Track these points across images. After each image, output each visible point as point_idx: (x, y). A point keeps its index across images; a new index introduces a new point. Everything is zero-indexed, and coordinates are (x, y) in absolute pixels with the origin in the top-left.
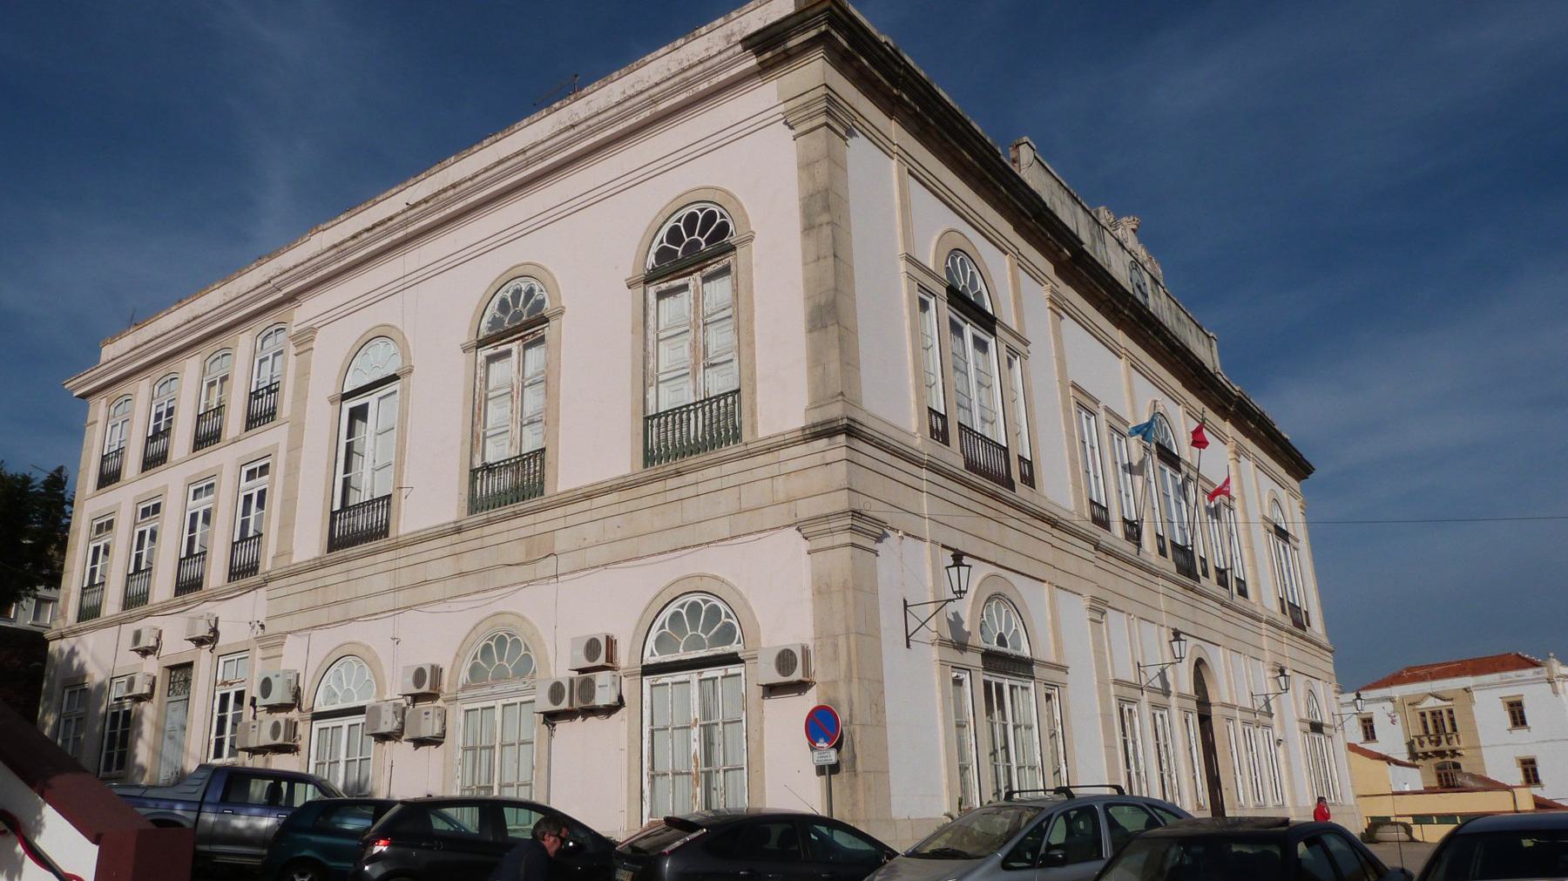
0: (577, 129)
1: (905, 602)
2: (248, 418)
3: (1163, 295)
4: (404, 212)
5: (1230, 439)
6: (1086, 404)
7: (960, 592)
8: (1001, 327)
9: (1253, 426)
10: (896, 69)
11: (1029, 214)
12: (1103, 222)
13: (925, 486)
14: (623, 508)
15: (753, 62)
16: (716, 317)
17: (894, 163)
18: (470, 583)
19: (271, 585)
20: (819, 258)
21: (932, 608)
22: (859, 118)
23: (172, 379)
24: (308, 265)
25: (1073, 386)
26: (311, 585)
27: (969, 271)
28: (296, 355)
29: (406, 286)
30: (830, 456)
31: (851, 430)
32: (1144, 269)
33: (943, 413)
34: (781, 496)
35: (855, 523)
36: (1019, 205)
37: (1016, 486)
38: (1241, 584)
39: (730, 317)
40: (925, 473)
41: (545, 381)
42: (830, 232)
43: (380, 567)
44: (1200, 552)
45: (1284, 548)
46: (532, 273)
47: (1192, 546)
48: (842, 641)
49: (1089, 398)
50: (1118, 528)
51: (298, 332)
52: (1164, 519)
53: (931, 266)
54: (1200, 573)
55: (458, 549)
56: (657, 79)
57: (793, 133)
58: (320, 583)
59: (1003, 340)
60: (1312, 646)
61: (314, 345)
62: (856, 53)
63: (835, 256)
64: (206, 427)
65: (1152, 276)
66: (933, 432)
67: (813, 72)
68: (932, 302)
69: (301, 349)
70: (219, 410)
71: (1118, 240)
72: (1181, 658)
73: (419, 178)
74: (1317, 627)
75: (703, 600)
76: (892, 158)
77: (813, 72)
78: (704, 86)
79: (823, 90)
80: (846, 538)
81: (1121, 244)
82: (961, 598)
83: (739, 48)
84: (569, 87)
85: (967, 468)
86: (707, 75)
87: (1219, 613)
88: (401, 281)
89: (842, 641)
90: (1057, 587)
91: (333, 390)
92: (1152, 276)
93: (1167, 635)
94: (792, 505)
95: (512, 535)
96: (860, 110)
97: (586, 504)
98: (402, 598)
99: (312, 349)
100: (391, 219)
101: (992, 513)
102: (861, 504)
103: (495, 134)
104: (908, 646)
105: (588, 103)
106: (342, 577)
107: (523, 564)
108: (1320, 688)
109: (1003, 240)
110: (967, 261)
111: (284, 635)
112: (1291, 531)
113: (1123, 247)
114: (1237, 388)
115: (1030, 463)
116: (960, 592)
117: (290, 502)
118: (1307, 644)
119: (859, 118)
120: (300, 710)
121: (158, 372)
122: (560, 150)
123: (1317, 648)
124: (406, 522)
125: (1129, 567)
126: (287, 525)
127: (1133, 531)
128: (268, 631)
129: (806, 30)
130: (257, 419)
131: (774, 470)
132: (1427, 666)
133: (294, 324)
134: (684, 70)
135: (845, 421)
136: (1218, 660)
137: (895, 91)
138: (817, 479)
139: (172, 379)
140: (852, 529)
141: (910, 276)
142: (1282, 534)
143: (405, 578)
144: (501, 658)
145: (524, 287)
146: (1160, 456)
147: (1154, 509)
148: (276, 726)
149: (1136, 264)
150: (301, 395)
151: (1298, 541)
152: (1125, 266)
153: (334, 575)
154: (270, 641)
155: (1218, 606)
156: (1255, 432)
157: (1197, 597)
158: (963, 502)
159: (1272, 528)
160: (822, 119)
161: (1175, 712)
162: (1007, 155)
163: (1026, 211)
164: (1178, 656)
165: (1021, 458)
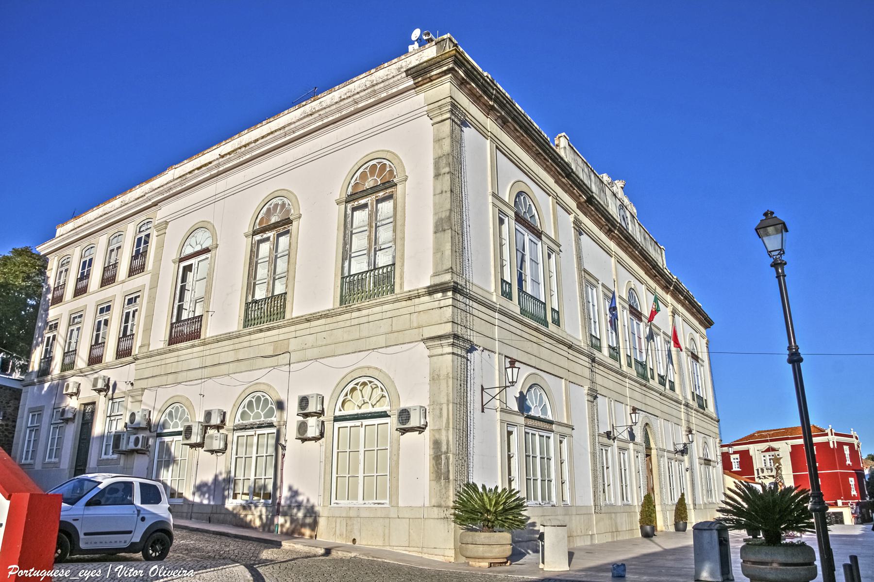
0: (313, 116)
1: (482, 386)
2: (130, 268)
3: (637, 225)
4: (217, 159)
5: (670, 305)
6: (587, 279)
7: (636, 423)
8: (545, 236)
9: (682, 298)
10: (491, 91)
11: (563, 174)
12: (605, 183)
13: (497, 322)
14: (327, 328)
15: (411, 82)
16: (384, 222)
17: (488, 142)
18: (242, 366)
19: (138, 362)
20: (442, 192)
21: (497, 390)
22: (469, 116)
23: (92, 248)
24: (165, 187)
25: (584, 271)
26: (159, 363)
27: (528, 204)
28: (157, 236)
29: (216, 200)
30: (443, 303)
31: (456, 289)
32: (627, 209)
33: (544, 302)
34: (415, 325)
35: (455, 341)
36: (558, 169)
37: (549, 325)
38: (672, 384)
39: (392, 222)
40: (497, 315)
41: (289, 255)
42: (449, 178)
43: (195, 355)
44: (650, 365)
45: (696, 365)
46: (284, 195)
47: (646, 362)
48: (445, 407)
49: (593, 278)
50: (606, 351)
51: (158, 224)
52: (632, 348)
53: (507, 200)
54: (649, 377)
55: (237, 346)
56: (358, 90)
57: (432, 122)
58: (163, 362)
59: (546, 243)
60: (708, 418)
61: (167, 231)
62: (468, 80)
63: (451, 191)
64: (108, 274)
65: (631, 214)
66: (503, 293)
67: (444, 88)
68: (506, 220)
69: (160, 233)
70: (115, 265)
71: (613, 193)
72: (636, 423)
73: (228, 141)
74: (711, 409)
75: (369, 381)
76: (488, 139)
77: (444, 88)
78: (384, 95)
79: (449, 100)
80: (449, 349)
81: (615, 195)
82: (513, 386)
83: (404, 75)
84: (313, 93)
85: (521, 313)
86: (385, 88)
87: (659, 399)
88: (214, 198)
89: (445, 407)
90: (569, 381)
91: (175, 256)
92: (631, 214)
93: (629, 410)
94: (421, 329)
95: (267, 340)
96: (470, 112)
97: (307, 325)
98: (206, 372)
99: (165, 233)
100: (210, 163)
101: (534, 339)
102: (460, 331)
103: (269, 118)
104: (483, 411)
105: (321, 103)
106: (175, 359)
107: (272, 356)
108: (711, 441)
109: (538, 178)
110: (527, 199)
111: (143, 390)
112: (700, 356)
113: (616, 197)
114: (675, 277)
115: (558, 312)
116: (513, 382)
117: (150, 317)
118: (706, 417)
119: (469, 116)
120: (150, 431)
121: (85, 243)
122: (303, 127)
123: (710, 419)
124: (209, 331)
125: (610, 372)
126: (148, 329)
127: (615, 352)
128: (135, 387)
129: (441, 67)
130: (135, 271)
131: (412, 309)
132: (768, 431)
133: (157, 219)
134: (373, 86)
135: (452, 284)
136: (658, 425)
137: (490, 103)
138: (436, 315)
139: (92, 248)
140: (453, 345)
141: (494, 205)
142: (695, 357)
143: (209, 361)
144: (258, 409)
145: (280, 202)
146: (631, 312)
147: (626, 341)
148: (137, 439)
149: (622, 206)
150: (158, 260)
151: (703, 361)
152: (616, 207)
153: (171, 358)
154: (136, 394)
155: (658, 395)
156: (683, 301)
157: (647, 390)
158: (518, 332)
159: (690, 354)
160: (448, 115)
161: (632, 452)
162: (554, 144)
163: (562, 173)
164: (634, 421)
165: (553, 310)
